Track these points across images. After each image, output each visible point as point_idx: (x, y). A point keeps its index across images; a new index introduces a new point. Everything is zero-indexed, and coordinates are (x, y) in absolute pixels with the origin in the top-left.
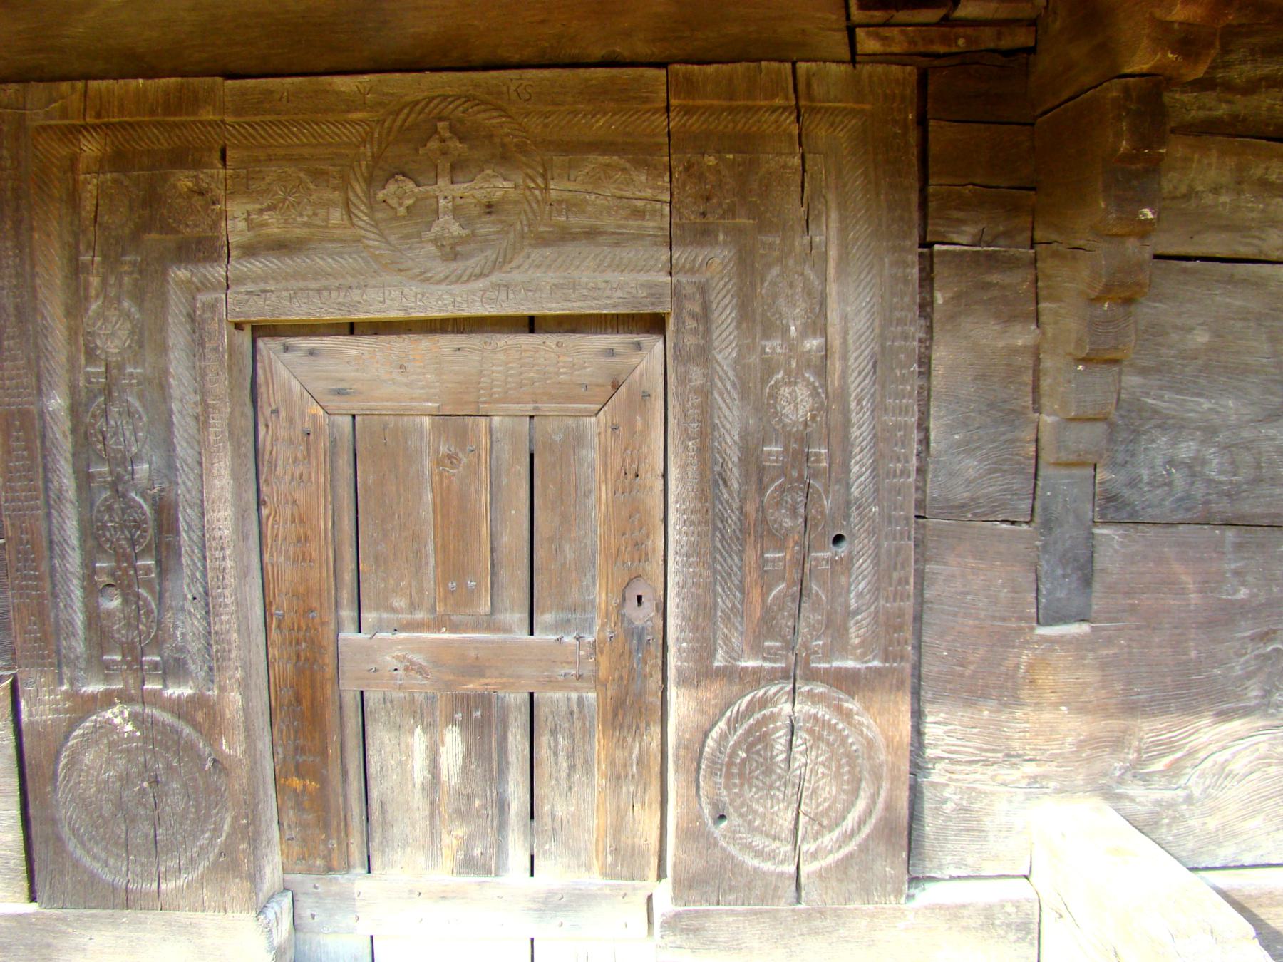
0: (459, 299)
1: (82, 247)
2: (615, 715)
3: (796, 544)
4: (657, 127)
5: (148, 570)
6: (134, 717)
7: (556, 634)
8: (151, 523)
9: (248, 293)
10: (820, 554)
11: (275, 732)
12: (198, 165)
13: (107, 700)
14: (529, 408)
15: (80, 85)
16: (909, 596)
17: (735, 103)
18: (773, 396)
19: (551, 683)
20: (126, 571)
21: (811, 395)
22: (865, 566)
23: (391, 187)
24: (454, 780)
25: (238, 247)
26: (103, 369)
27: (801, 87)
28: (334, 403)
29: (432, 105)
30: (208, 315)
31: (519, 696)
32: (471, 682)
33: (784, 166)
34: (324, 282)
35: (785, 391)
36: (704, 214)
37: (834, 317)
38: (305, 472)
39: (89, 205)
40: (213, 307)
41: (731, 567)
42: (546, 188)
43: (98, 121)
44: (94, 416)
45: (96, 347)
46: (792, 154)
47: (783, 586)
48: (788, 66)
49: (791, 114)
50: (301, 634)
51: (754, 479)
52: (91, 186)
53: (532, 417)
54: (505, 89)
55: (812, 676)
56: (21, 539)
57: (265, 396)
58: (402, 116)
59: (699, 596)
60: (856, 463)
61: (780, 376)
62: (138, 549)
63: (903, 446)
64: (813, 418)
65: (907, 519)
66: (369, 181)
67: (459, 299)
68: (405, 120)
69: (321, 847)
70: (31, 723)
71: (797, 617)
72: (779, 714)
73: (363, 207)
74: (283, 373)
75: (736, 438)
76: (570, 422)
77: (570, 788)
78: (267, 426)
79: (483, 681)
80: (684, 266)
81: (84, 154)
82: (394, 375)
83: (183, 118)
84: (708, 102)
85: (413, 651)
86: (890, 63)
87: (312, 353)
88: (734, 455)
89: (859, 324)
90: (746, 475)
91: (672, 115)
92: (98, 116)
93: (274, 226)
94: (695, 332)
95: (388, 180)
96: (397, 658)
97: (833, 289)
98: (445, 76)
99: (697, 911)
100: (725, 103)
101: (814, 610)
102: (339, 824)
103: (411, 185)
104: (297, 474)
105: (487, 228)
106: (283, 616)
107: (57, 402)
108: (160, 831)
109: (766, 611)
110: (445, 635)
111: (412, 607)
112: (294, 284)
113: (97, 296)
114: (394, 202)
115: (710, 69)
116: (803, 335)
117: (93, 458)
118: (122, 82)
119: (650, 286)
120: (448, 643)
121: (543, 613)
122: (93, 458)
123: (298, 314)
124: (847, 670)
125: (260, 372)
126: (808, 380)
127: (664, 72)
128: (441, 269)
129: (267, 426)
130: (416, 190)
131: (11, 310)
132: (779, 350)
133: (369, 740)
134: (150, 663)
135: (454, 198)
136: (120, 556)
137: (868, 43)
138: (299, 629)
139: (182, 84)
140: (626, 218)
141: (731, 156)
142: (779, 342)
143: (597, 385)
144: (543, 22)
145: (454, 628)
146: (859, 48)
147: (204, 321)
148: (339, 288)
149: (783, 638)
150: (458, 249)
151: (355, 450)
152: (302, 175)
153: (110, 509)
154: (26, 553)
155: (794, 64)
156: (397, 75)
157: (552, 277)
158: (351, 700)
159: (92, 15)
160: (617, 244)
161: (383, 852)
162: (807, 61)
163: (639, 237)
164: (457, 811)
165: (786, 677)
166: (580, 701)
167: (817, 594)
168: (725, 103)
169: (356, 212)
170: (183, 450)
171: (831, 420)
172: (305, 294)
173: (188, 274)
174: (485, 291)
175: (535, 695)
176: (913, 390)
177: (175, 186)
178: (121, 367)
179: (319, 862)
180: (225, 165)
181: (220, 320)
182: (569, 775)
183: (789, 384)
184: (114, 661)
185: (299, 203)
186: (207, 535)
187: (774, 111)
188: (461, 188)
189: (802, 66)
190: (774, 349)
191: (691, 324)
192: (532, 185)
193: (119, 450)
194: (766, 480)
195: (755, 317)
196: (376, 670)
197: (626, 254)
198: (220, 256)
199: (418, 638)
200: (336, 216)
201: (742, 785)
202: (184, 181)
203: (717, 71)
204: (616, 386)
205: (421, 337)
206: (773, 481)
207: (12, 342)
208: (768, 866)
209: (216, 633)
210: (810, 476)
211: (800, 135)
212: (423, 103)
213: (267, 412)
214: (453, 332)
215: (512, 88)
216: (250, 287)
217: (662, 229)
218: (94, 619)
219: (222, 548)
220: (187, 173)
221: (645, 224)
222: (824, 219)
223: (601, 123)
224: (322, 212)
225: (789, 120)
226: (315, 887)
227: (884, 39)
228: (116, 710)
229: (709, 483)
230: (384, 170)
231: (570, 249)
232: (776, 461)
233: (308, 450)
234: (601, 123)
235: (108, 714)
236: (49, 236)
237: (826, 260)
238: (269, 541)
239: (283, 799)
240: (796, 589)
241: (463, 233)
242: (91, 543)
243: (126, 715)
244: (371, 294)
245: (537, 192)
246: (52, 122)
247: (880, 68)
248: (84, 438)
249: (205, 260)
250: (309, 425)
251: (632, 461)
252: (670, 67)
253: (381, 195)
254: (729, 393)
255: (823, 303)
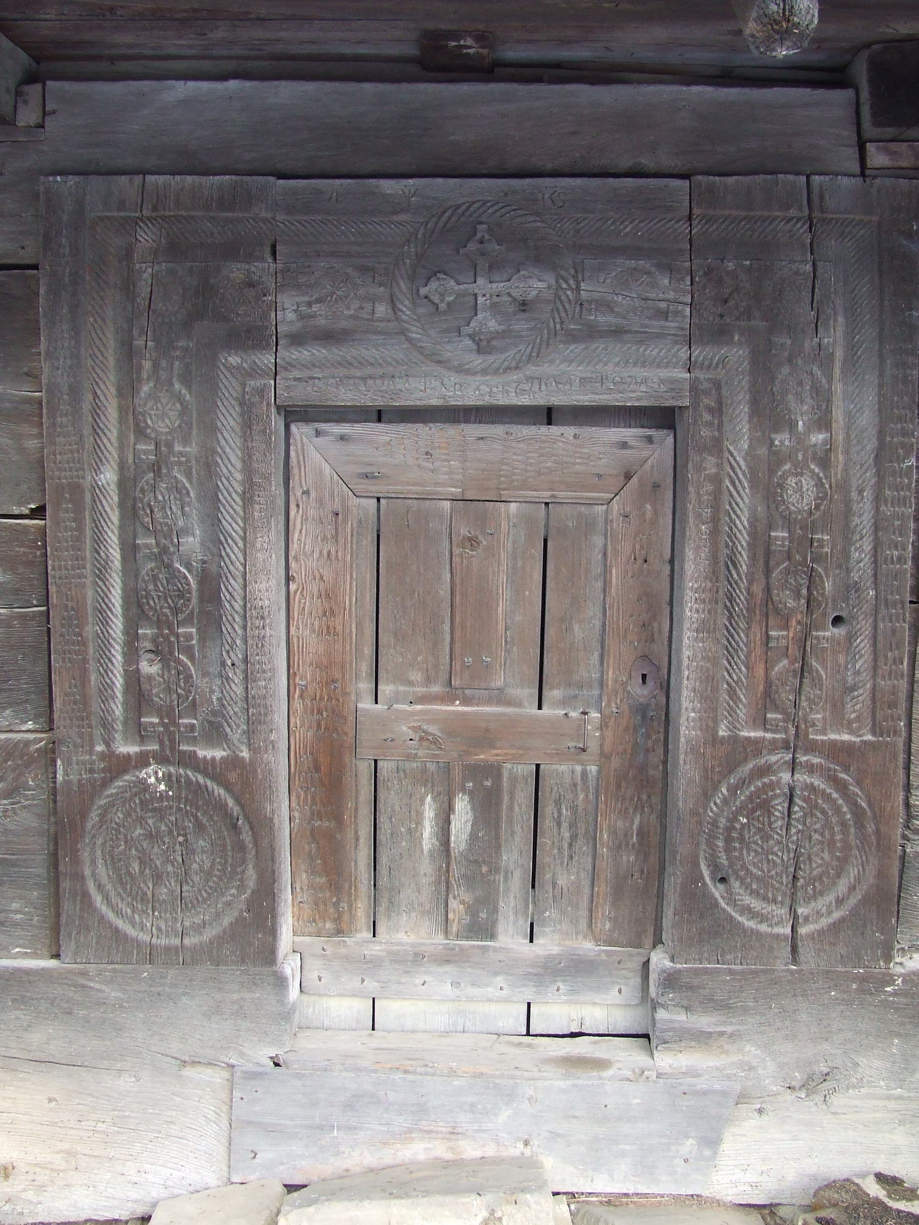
0: (495, 390)
1: (136, 333)
2: (619, 786)
3: (799, 623)
4: (679, 234)
5: (189, 637)
6: (168, 778)
7: (564, 709)
8: (195, 594)
9: (296, 379)
10: (821, 633)
11: (293, 798)
12: (250, 258)
13: (143, 760)
14: (545, 495)
15: (138, 179)
16: (902, 675)
17: (752, 213)
18: (781, 486)
19: (561, 756)
20: (167, 638)
21: (816, 485)
22: (862, 645)
23: (433, 285)
24: (463, 846)
25: (286, 336)
26: (153, 447)
27: (815, 197)
28: (362, 486)
29: (472, 209)
30: (257, 399)
31: (526, 767)
32: (483, 753)
33: (797, 273)
34: (369, 370)
35: (792, 481)
36: (722, 316)
37: (838, 415)
38: (333, 552)
39: (143, 290)
40: (261, 392)
41: (737, 643)
42: (578, 289)
43: (154, 214)
44: (143, 491)
45: (147, 426)
46: (804, 262)
47: (785, 662)
48: (803, 179)
49: (804, 224)
50: (323, 704)
51: (761, 562)
52: (146, 274)
53: (547, 504)
54: (540, 195)
55: (812, 747)
56: (66, 606)
57: (297, 478)
58: (444, 219)
59: (708, 670)
60: (856, 549)
61: (787, 467)
62: (181, 617)
63: (901, 535)
64: (817, 507)
65: (902, 602)
66: (412, 278)
67: (495, 390)
68: (446, 223)
69: (332, 910)
70: (67, 783)
71: (799, 692)
72: (779, 782)
73: (407, 302)
74: (314, 457)
75: (746, 523)
76: (583, 509)
77: (571, 857)
78: (298, 506)
79: (494, 752)
80: (702, 364)
81: (138, 245)
82: (420, 462)
83: (235, 215)
84: (727, 212)
85: (430, 722)
86: (897, 177)
87: (342, 438)
88: (743, 539)
89: (867, 419)
90: (753, 558)
91: (695, 223)
92: (155, 208)
93: (322, 316)
94: (710, 424)
95: (429, 279)
96: (413, 728)
97: (838, 388)
98: (483, 182)
99: (696, 969)
100: (743, 214)
101: (813, 685)
102: (350, 888)
103: (452, 283)
104: (325, 552)
105: (521, 325)
106: (306, 686)
107: (109, 477)
108: (185, 888)
109: (768, 683)
110: (458, 707)
111: (428, 681)
112: (342, 372)
113: (148, 379)
114: (436, 298)
115: (731, 180)
116: (808, 431)
117: (140, 530)
118: (178, 178)
119: (672, 381)
120: (463, 714)
121: (552, 688)
122: (140, 530)
123: (343, 400)
124: (843, 742)
125: (292, 454)
126: (812, 471)
127: (687, 182)
128: (478, 361)
129: (298, 506)
130: (456, 288)
131: (65, 389)
132: (787, 443)
133: (380, 806)
134: (186, 726)
135: (491, 296)
136: (160, 623)
137: (877, 158)
138: (321, 698)
139: (236, 182)
140: (650, 318)
141: (748, 263)
142: (788, 436)
143: (610, 475)
144: (574, 133)
145: (466, 701)
146: (869, 163)
147: (252, 404)
148: (382, 377)
149: (784, 712)
150: (494, 343)
151: (378, 531)
152: (349, 270)
153: (155, 578)
154: (70, 618)
155: (808, 177)
156: (441, 180)
157: (578, 371)
158: (364, 769)
159: (146, 112)
160: (640, 343)
161: (389, 917)
162: (820, 174)
163: (660, 336)
164: (465, 876)
165: (787, 748)
166: (584, 774)
167: (817, 671)
168: (743, 214)
169: (400, 306)
170: (232, 526)
171: (834, 512)
172: (351, 381)
173: (239, 360)
174: (519, 383)
175: (542, 767)
176: (910, 483)
177: (228, 278)
178: (169, 445)
179: (328, 925)
180: (275, 259)
181: (268, 404)
182: (570, 845)
183: (797, 475)
184: (152, 723)
185: (346, 297)
186: (249, 605)
187: (788, 222)
188: (499, 287)
189: (816, 179)
190: (782, 442)
191: (707, 417)
192: (564, 286)
193: (167, 524)
194: (772, 563)
195: (769, 413)
196: (393, 740)
197: (652, 351)
198: (268, 344)
199: (435, 710)
200: (382, 310)
201: (741, 849)
202: (236, 271)
203: (737, 181)
204: (628, 476)
205: (447, 425)
206: (778, 564)
207: (65, 419)
208: (763, 928)
209: (254, 697)
210: (812, 561)
211: (811, 244)
212: (464, 207)
213: (299, 493)
214: (475, 422)
215: (547, 196)
216: (296, 374)
217: (682, 329)
218: (134, 680)
219: (263, 618)
220: (239, 265)
221: (667, 324)
222: (832, 322)
223: (628, 229)
224: (368, 306)
225: (802, 229)
226: (323, 949)
227: (893, 154)
228: (150, 770)
229: (722, 565)
230: (427, 269)
231: (599, 346)
232: (783, 545)
233: (336, 529)
234: (628, 229)
235: (143, 775)
236: (104, 320)
237: (833, 361)
238: (296, 615)
239: (297, 863)
240: (798, 665)
241: (500, 328)
242: (134, 610)
243: (160, 774)
244: (414, 383)
245: (569, 293)
246: (108, 214)
247: (888, 182)
248: (131, 510)
249: (253, 347)
250: (337, 506)
251: (642, 547)
252: (694, 178)
253: (423, 291)
254: (740, 481)
255: (829, 402)
